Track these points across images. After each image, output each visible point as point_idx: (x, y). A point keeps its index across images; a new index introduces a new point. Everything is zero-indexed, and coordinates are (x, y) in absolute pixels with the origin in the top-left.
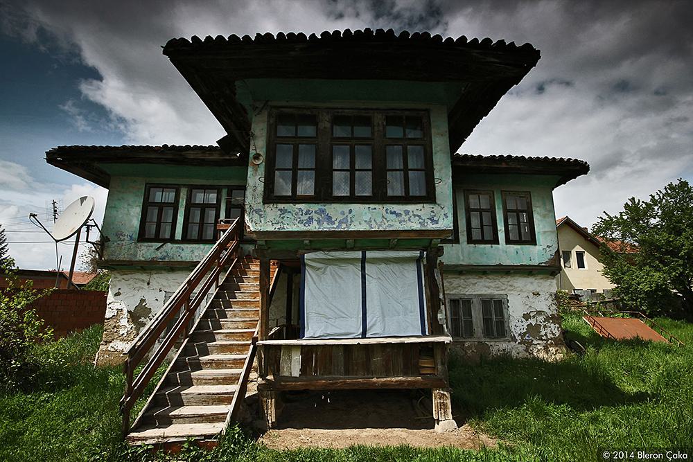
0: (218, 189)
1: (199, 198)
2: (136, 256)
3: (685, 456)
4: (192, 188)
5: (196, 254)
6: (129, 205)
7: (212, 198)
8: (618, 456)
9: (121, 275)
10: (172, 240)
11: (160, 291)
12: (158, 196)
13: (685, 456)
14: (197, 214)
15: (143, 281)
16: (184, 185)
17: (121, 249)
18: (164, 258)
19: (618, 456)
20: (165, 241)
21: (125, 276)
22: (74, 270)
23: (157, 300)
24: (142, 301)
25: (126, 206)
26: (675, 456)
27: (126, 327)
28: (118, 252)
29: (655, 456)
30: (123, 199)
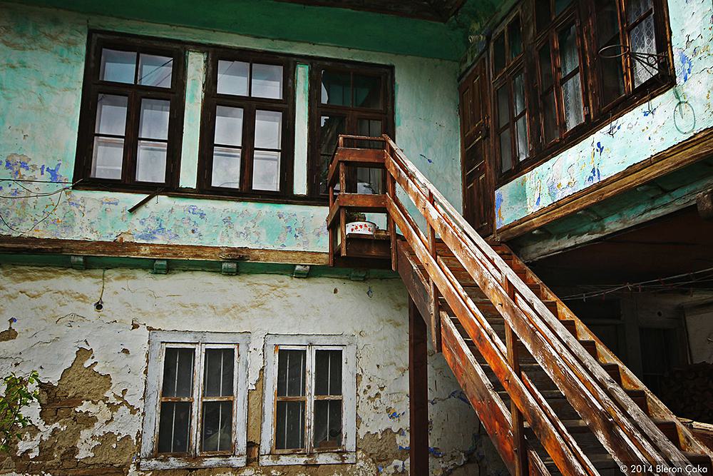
0: (288, 64)
1: (231, 83)
2: (71, 227)
3: (705, 470)
4: (216, 55)
5: (240, 228)
6: (42, 84)
7: (271, 89)
8: (635, 470)
9: (17, 281)
10: (171, 187)
11: (135, 326)
12: (119, 70)
13: (705, 470)
14: (228, 128)
15: (83, 298)
16: (199, 47)
17: (24, 205)
18: (151, 235)
19: (635, 470)
20: (152, 189)
21: (27, 285)
22: (135, 65)
23: (126, 351)
24: (83, 353)
25: (34, 88)
26: (695, 470)
27: (35, 430)
28: (13, 215)
29: (674, 470)
30: (24, 65)
